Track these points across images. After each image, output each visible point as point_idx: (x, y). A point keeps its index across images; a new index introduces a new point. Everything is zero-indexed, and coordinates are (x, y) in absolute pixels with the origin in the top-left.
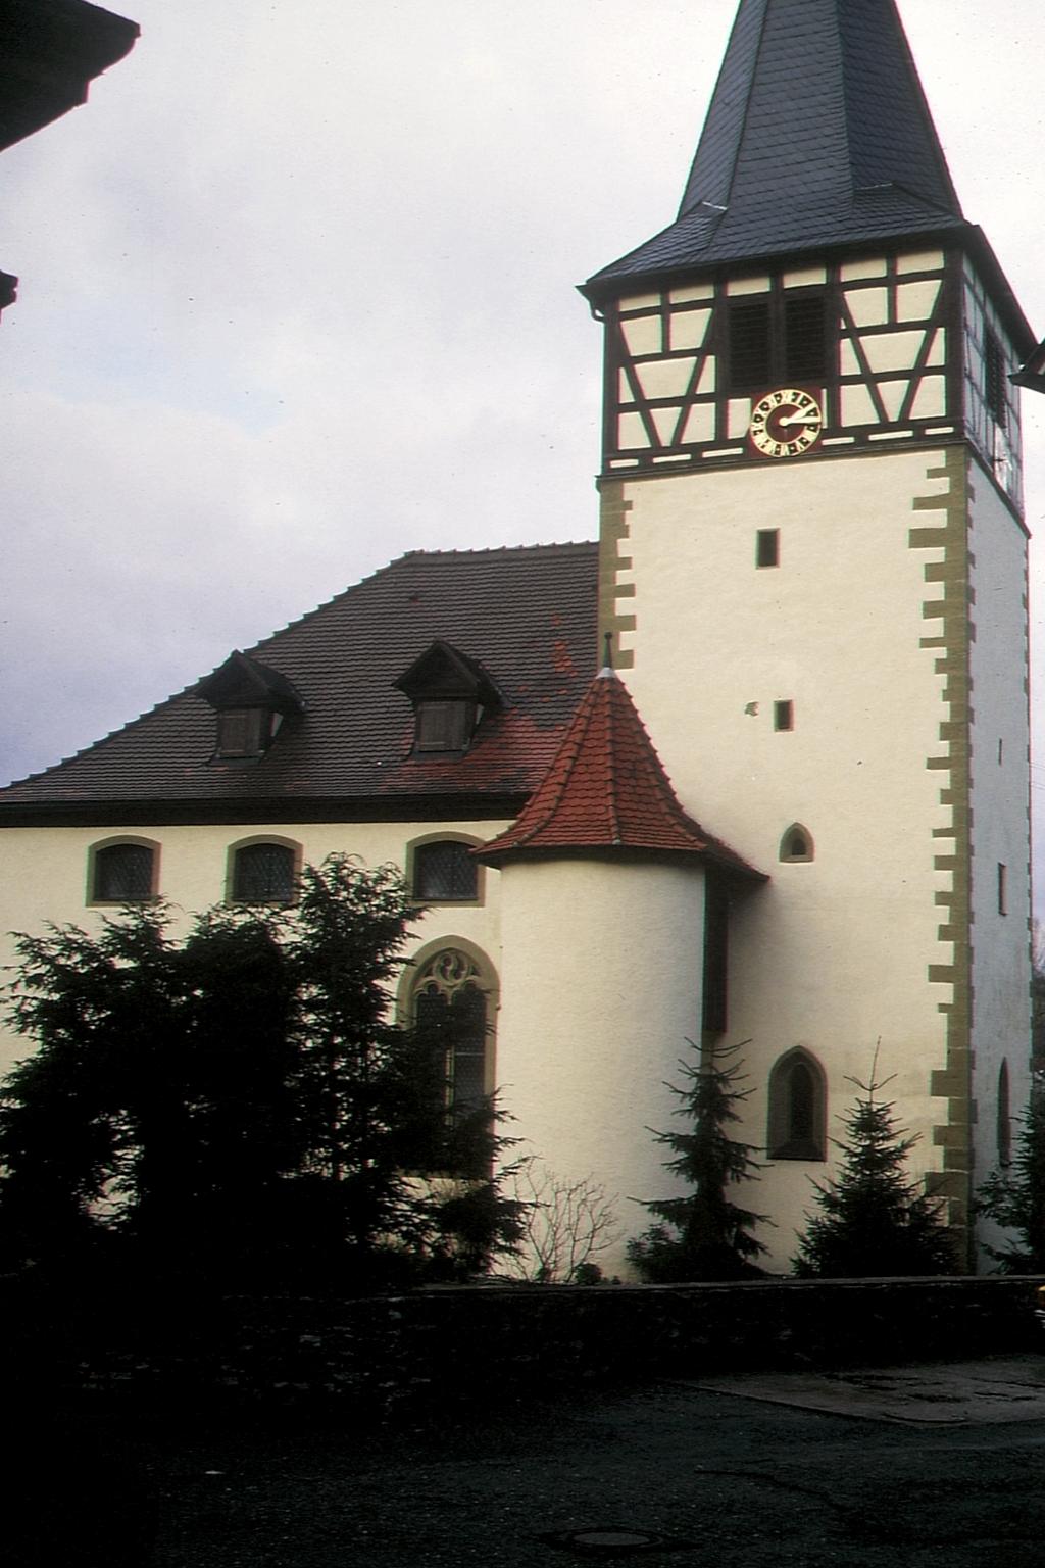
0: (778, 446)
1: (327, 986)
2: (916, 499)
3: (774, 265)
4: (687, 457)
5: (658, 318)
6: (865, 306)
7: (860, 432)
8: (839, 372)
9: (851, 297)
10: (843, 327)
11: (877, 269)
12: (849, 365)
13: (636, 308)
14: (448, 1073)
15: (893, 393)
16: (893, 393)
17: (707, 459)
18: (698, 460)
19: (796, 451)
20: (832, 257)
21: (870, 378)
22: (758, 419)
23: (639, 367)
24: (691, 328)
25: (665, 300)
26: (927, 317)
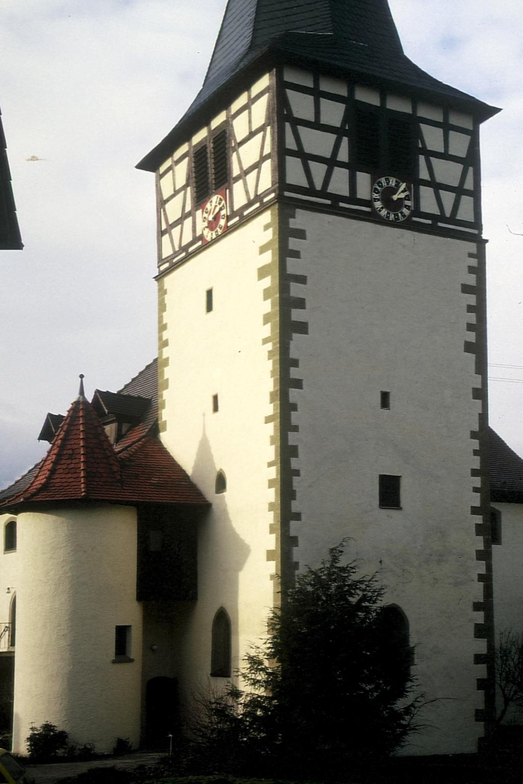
1: (278, 700)
4: (329, 202)
7: (336, 198)
10: (347, 128)
14: (167, 754)
15: (318, 170)
21: (437, 187)
22: (376, 191)
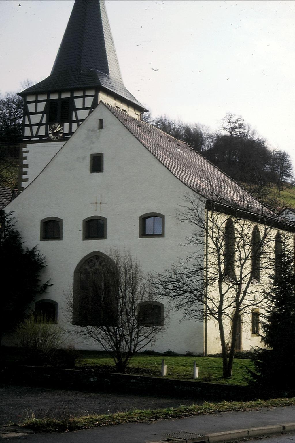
0: (54, 137)
2: (28, 152)
3: (60, 92)
5: (82, 99)
6: (78, 103)
8: (72, 119)
9: (75, 100)
11: (81, 94)
12: (74, 118)
13: (65, 97)
16: (35, 129)
17: (66, 137)
18: (42, 139)
19: (58, 138)
20: (72, 91)
23: (78, 112)
24: (41, 107)
25: (37, 98)
26: (42, 111)
